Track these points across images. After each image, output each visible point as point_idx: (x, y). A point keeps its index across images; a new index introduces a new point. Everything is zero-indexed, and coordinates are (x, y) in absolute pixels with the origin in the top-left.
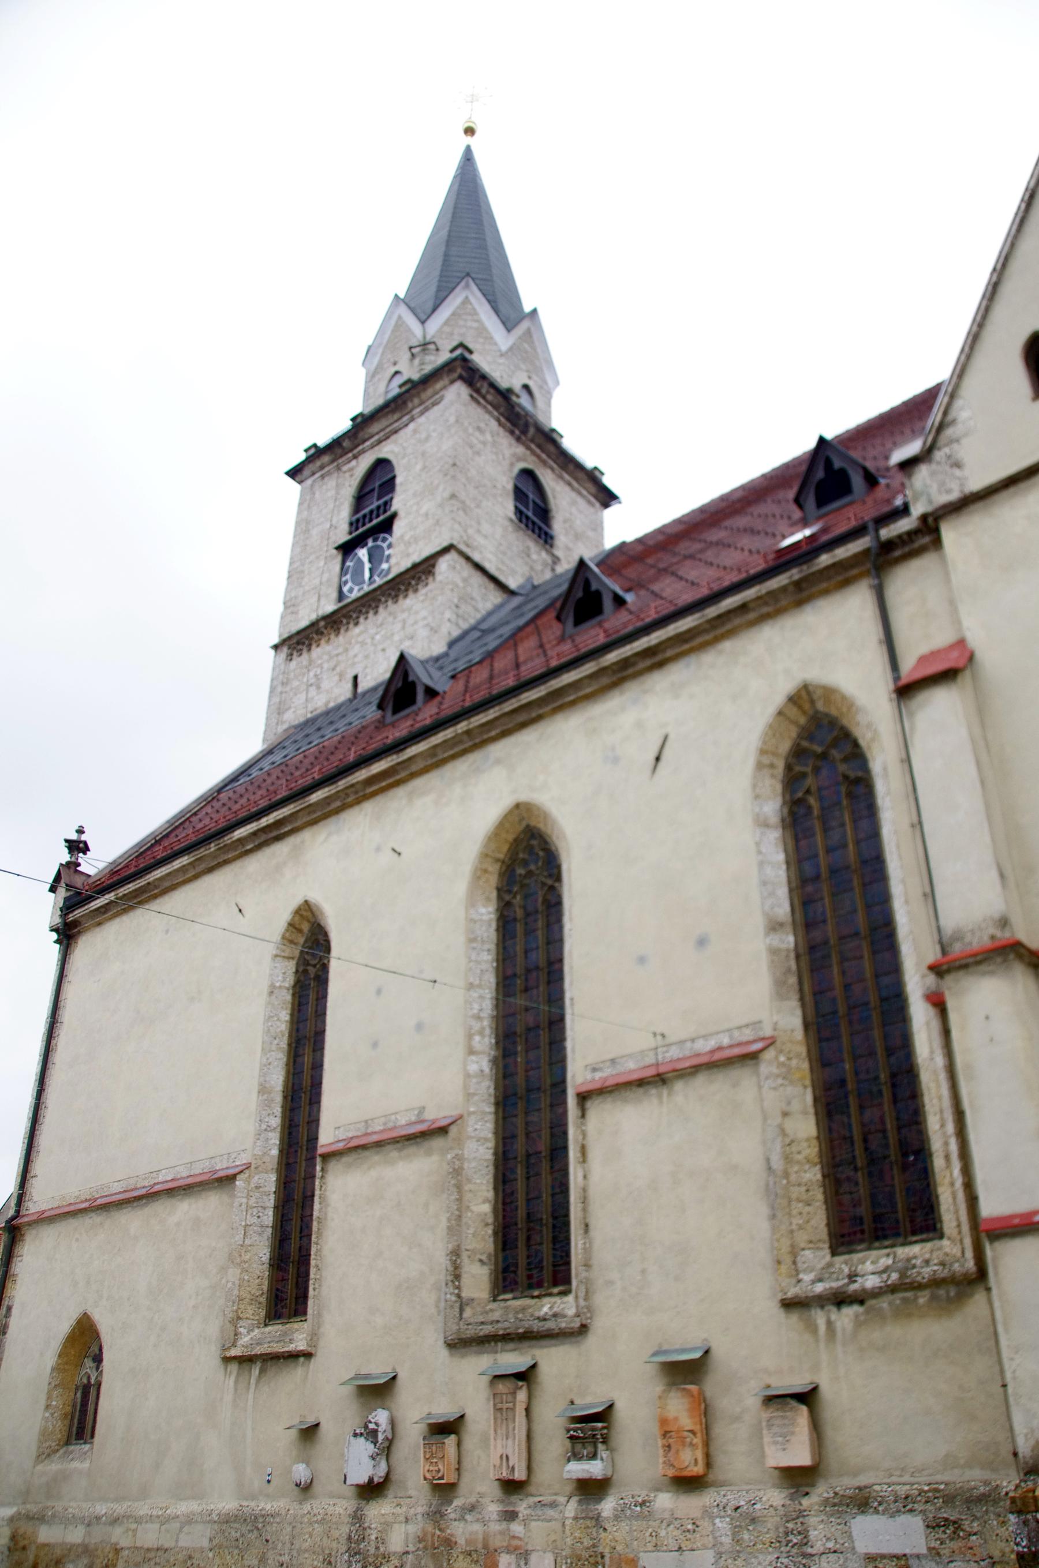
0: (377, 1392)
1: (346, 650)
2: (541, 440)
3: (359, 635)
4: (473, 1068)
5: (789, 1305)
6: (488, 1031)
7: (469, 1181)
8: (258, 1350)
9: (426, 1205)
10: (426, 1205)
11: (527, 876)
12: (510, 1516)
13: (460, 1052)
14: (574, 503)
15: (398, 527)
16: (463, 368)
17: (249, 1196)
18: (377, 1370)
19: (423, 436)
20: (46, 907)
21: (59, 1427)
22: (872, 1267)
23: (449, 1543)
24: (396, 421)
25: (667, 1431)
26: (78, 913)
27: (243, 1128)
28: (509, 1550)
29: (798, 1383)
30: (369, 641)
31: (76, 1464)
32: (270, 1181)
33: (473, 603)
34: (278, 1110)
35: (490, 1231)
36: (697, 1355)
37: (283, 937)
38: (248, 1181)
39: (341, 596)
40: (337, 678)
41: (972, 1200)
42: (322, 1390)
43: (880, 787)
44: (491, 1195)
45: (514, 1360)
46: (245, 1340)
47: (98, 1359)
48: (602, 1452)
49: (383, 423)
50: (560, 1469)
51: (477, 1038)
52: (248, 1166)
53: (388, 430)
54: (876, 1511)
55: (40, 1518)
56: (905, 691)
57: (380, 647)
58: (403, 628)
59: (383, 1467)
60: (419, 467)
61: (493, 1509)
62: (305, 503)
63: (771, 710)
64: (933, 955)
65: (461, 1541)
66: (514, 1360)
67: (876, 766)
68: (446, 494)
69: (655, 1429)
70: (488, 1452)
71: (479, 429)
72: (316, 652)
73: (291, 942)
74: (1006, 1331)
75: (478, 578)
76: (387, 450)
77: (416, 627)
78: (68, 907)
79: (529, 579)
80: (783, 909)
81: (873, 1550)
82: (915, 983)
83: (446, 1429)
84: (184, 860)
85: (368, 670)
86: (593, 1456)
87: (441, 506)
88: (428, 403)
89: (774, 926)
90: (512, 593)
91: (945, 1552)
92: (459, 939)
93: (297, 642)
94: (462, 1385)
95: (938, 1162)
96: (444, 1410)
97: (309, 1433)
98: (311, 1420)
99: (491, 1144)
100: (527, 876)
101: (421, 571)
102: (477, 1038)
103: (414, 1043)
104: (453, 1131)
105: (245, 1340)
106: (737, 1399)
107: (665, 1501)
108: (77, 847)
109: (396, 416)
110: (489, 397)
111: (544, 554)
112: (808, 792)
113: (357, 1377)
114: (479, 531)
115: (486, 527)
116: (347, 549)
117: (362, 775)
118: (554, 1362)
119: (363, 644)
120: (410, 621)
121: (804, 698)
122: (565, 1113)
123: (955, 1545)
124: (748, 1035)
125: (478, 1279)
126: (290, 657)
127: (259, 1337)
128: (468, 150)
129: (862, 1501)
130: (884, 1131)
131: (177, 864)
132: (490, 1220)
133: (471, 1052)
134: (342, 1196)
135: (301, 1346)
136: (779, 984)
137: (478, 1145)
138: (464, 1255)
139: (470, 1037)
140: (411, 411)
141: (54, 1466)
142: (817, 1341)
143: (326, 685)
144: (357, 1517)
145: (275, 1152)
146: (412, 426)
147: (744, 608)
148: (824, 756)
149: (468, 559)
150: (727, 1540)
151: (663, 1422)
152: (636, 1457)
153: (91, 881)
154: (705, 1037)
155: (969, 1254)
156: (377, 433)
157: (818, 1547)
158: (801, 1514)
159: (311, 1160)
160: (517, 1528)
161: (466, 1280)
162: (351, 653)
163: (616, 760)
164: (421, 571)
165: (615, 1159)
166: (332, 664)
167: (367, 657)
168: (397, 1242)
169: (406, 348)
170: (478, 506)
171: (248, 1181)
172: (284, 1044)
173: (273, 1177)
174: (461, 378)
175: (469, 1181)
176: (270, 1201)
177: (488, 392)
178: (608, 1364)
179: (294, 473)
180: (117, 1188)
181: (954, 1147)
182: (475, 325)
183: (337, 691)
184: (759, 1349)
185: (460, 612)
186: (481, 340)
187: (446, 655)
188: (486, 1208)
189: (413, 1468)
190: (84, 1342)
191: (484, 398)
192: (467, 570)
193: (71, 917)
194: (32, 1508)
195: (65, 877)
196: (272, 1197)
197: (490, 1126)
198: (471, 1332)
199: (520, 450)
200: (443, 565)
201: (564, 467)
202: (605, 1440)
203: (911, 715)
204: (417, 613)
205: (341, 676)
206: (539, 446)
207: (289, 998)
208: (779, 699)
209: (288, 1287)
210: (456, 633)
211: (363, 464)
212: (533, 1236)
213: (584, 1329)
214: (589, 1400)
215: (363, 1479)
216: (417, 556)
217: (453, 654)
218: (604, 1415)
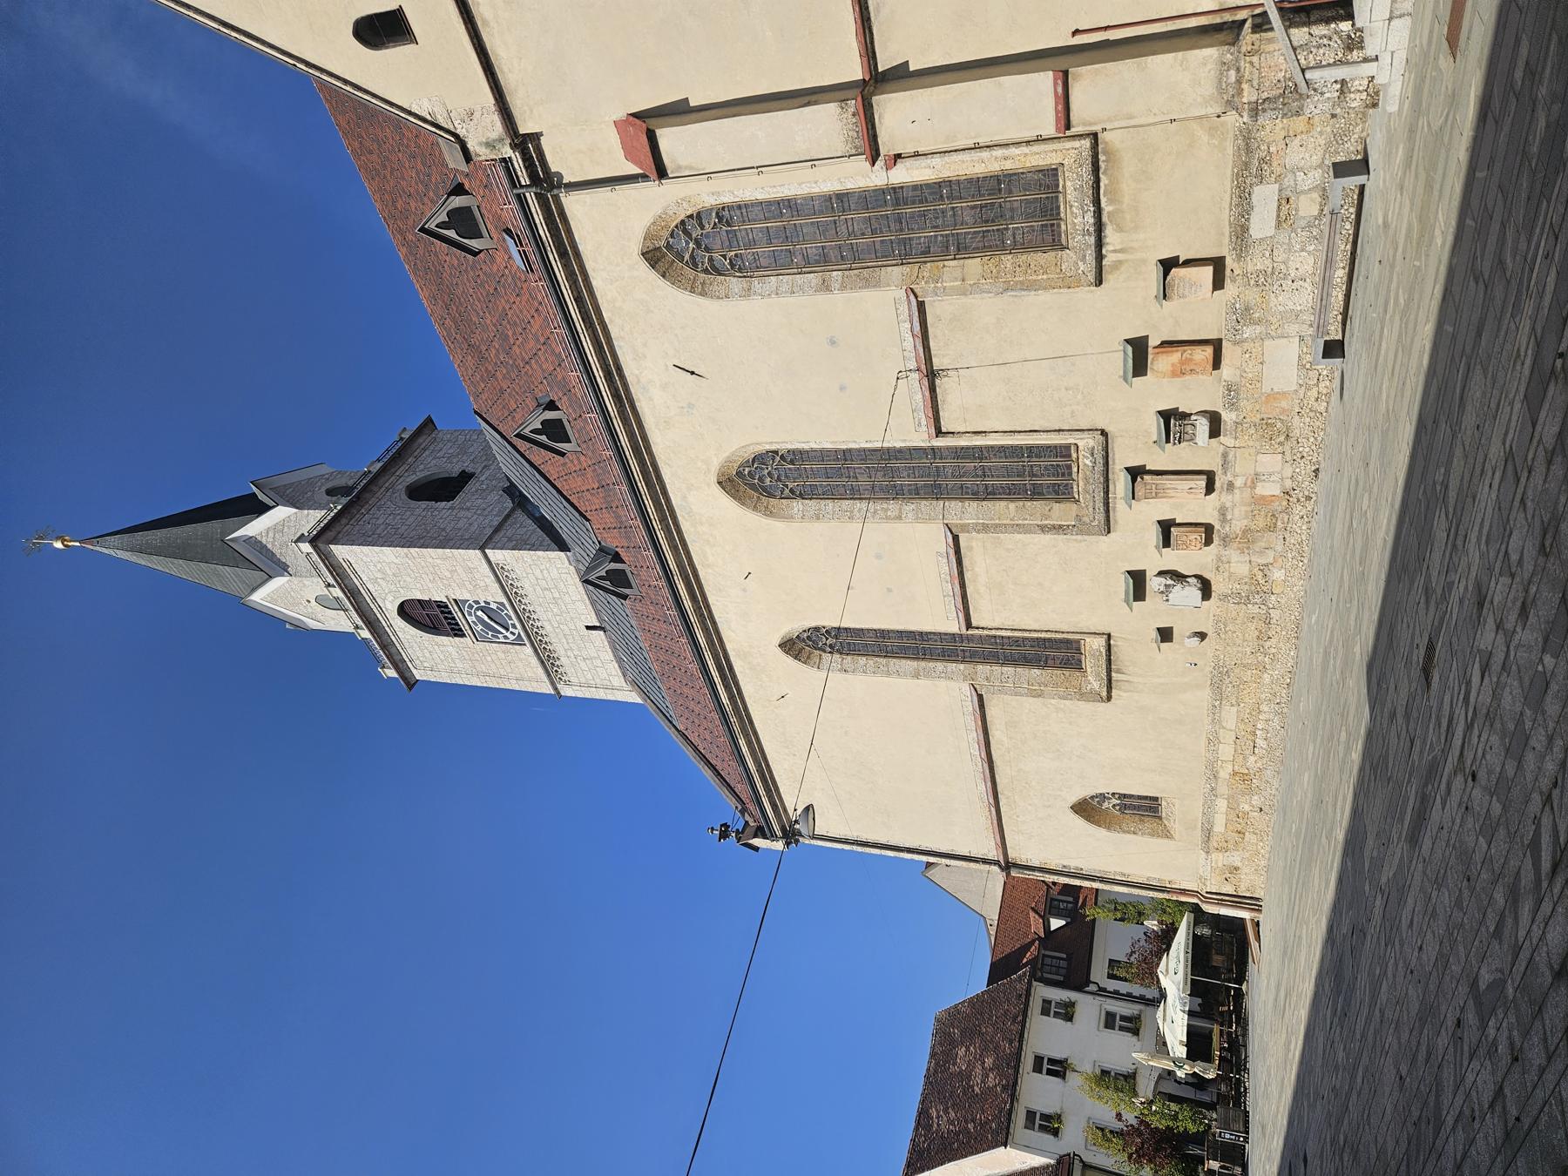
5: (1099, 281)
9: (1008, 550)
10: (1008, 550)
11: (764, 479)
12: (1231, 486)
13: (898, 526)
18: (1123, 585)
19: (379, 575)
21: (1149, 824)
22: (1076, 218)
23: (1246, 531)
25: (1179, 372)
26: (776, 828)
27: (943, 692)
28: (1253, 487)
29: (1155, 273)
32: (983, 669)
36: (1130, 349)
39: (518, 642)
41: (1039, 140)
43: (727, 199)
45: (1120, 482)
46: (1096, 685)
47: (1103, 797)
50: (1199, 451)
54: (1248, 220)
56: (662, 173)
59: (1192, 580)
61: (1227, 499)
63: (661, 282)
64: (862, 163)
65: (1245, 522)
66: (1120, 482)
67: (709, 201)
69: (1178, 380)
70: (1187, 503)
74: (1131, 117)
76: (391, 608)
80: (813, 279)
81: (1273, 224)
82: (876, 177)
84: (742, 742)
89: (825, 287)
91: (1278, 170)
92: (817, 527)
94: (1137, 519)
95: (1008, 165)
97: (1165, 635)
100: (764, 479)
103: (889, 565)
106: (1160, 324)
107: (1226, 371)
112: (724, 257)
113: (1127, 601)
114: (467, 530)
117: (688, 604)
121: (652, 257)
122: (948, 448)
123: (1275, 164)
124: (904, 308)
125: (1060, 512)
129: (1241, 232)
130: (982, 206)
131: (745, 749)
134: (992, 615)
136: (868, 284)
137: (966, 512)
139: (887, 518)
147: (579, 300)
148: (698, 243)
150: (1258, 329)
151: (1174, 374)
152: (1196, 392)
154: (902, 341)
155: (1077, 144)
157: (1268, 262)
158: (1245, 275)
159: (970, 639)
160: (1239, 482)
163: (691, 406)
165: (984, 410)
168: (1036, 574)
172: (883, 661)
173: (980, 667)
176: (997, 669)
178: (1129, 414)
181: (999, 152)
184: (1130, 303)
188: (1012, 506)
189: (1189, 557)
190: (1087, 809)
193: (779, 833)
203: (679, 168)
208: (652, 276)
209: (1053, 654)
211: (400, 625)
212: (1032, 475)
213: (1104, 433)
214: (1154, 430)
215: (1199, 594)
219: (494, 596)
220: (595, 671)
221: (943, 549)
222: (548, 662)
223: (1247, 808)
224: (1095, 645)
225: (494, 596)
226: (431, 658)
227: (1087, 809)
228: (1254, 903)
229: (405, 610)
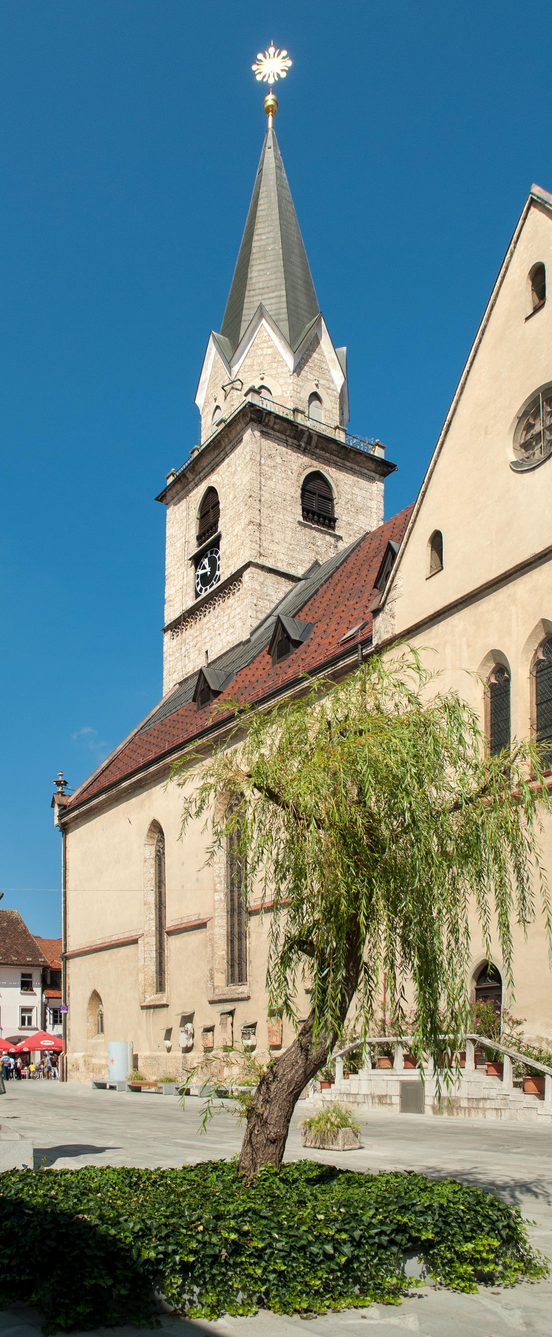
0: (188, 1019)
1: (201, 634)
3: (206, 623)
4: (217, 898)
6: (223, 882)
7: (216, 943)
8: (152, 1003)
15: (223, 543)
16: (251, 412)
17: (144, 947)
24: (217, 456)
30: (212, 627)
31: (100, 1040)
33: (268, 598)
34: (153, 912)
35: (225, 961)
37: (148, 836)
38: (143, 941)
39: (197, 595)
40: (197, 652)
42: (172, 1018)
44: (226, 947)
45: (228, 1007)
46: (148, 999)
48: (252, 1037)
51: (218, 885)
52: (143, 935)
53: (212, 464)
55: (92, 1056)
57: (218, 632)
58: (229, 620)
60: (231, 496)
66: (228, 1007)
68: (247, 521)
73: (152, 837)
75: (272, 578)
77: (235, 619)
83: (210, 1030)
85: (213, 648)
86: (249, 1039)
87: (243, 530)
88: (234, 442)
90: (299, 580)
96: (209, 1024)
98: (170, 1027)
99: (225, 928)
101: (237, 577)
102: (218, 885)
104: (209, 924)
105: (148, 999)
109: (216, 453)
110: (276, 427)
111: (328, 538)
113: (183, 1013)
115: (278, 536)
116: (197, 560)
118: (240, 1008)
119: (209, 629)
120: (232, 615)
127: (152, 998)
132: (226, 957)
133: (216, 891)
135: (164, 1002)
138: (215, 971)
140: (225, 448)
141: (93, 1041)
143: (192, 656)
144: (184, 1057)
145: (154, 928)
146: (227, 461)
149: (263, 568)
156: (207, 466)
161: (216, 980)
162: (204, 635)
164: (237, 577)
166: (195, 642)
167: (211, 639)
169: (220, 389)
170: (271, 522)
171: (143, 941)
173: (154, 939)
174: (252, 420)
175: (216, 943)
176: (154, 948)
177: (275, 423)
180: (99, 942)
182: (270, 351)
183: (198, 661)
185: (259, 608)
186: (275, 365)
187: (248, 641)
188: (224, 953)
189: (199, 1041)
190: (96, 997)
191: (273, 429)
192: (263, 575)
193: (65, 819)
194: (89, 1053)
196: (154, 946)
197: (225, 921)
198: (216, 998)
199: (306, 460)
200: (246, 575)
201: (346, 458)
202: (254, 1034)
204: (235, 609)
205: (199, 650)
206: (323, 449)
207: (154, 862)
210: (256, 623)
211: (201, 490)
215: (185, 1046)
216: (233, 570)
217: (253, 639)
218: (254, 1026)
219: (224, 573)
220: (182, 658)
221: (202, 917)
222: (177, 625)
223: (103, 1073)
224: (242, 990)
225: (224, 573)
226: (181, 522)
227: (96, 997)
228: (64, 1079)
229: (211, 492)
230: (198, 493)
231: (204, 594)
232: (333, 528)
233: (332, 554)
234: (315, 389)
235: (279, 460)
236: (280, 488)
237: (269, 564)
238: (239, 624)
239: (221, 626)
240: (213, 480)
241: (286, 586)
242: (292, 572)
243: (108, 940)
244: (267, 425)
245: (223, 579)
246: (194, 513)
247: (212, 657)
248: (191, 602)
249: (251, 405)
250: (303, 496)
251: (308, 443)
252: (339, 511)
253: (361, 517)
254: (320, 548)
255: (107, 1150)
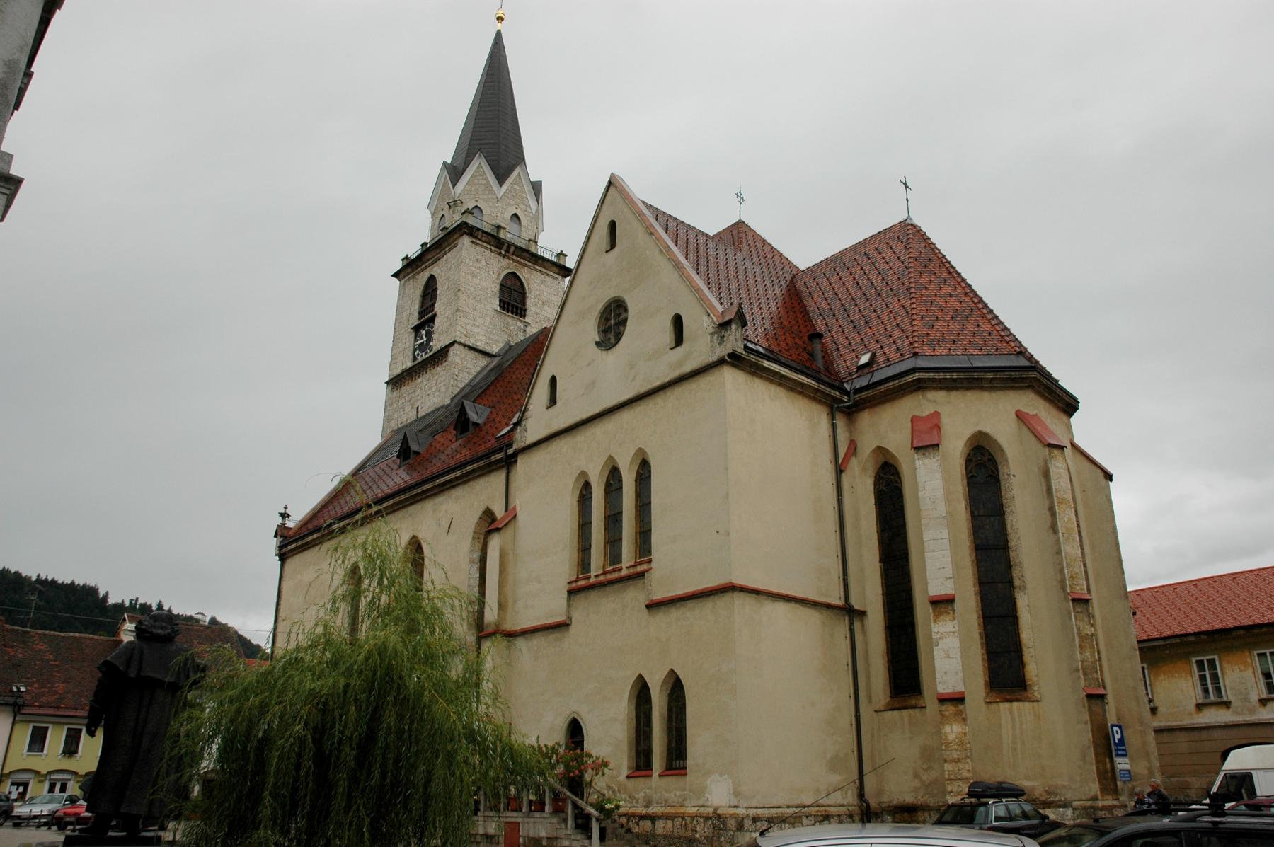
2: (518, 252)
14: (543, 282)
15: (437, 321)
20: (273, 543)
39: (415, 359)
49: (433, 253)
62: (402, 288)
71: (477, 260)
72: (403, 389)
75: (472, 354)
78: (281, 547)
79: (508, 343)
93: (396, 382)
108: (284, 516)
116: (417, 329)
126: (393, 390)
128: (499, 34)
142: (590, 838)
143: (407, 409)
149: (465, 346)
153: (291, 533)
179: (396, 275)
193: (284, 550)
195: (281, 532)
199: (505, 262)
208: (480, 513)
216: (443, 344)
225: (437, 345)
229: (432, 278)
230: (424, 277)
231: (420, 359)
232: (524, 317)
233: (521, 337)
234: (516, 211)
235: (483, 263)
236: (484, 284)
237: (471, 342)
238: (443, 389)
239: (431, 388)
240: (435, 270)
241: (482, 362)
242: (488, 349)
243: (659, 400)
244: (476, 237)
245: (435, 349)
246: (419, 292)
247: (422, 413)
248: (409, 364)
249: (464, 223)
250: (501, 291)
251: (508, 251)
252: (530, 303)
253: (546, 308)
254: (513, 332)
255: (736, 594)
